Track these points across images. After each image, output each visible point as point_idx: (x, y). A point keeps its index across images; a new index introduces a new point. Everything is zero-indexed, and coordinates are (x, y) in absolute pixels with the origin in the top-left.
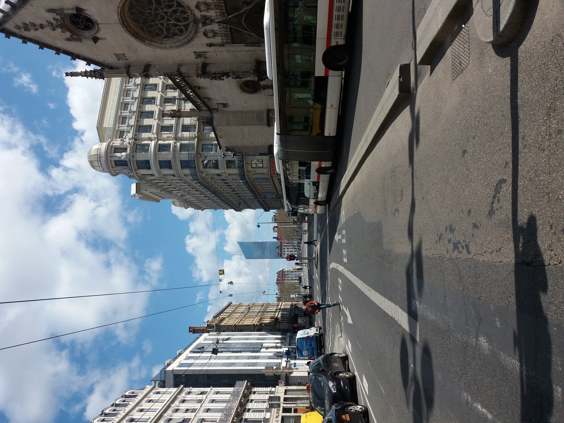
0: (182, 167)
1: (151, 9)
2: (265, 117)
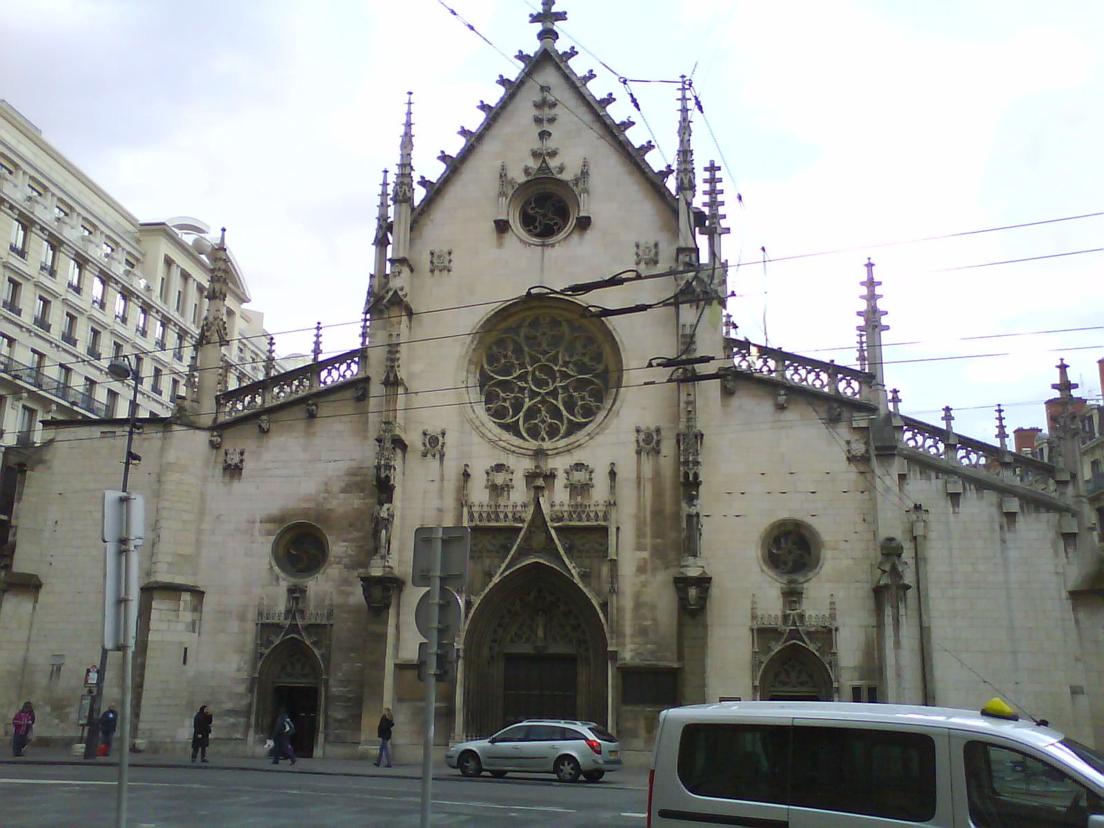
0: (1040, 450)
1: (566, 364)
2: (179, 580)
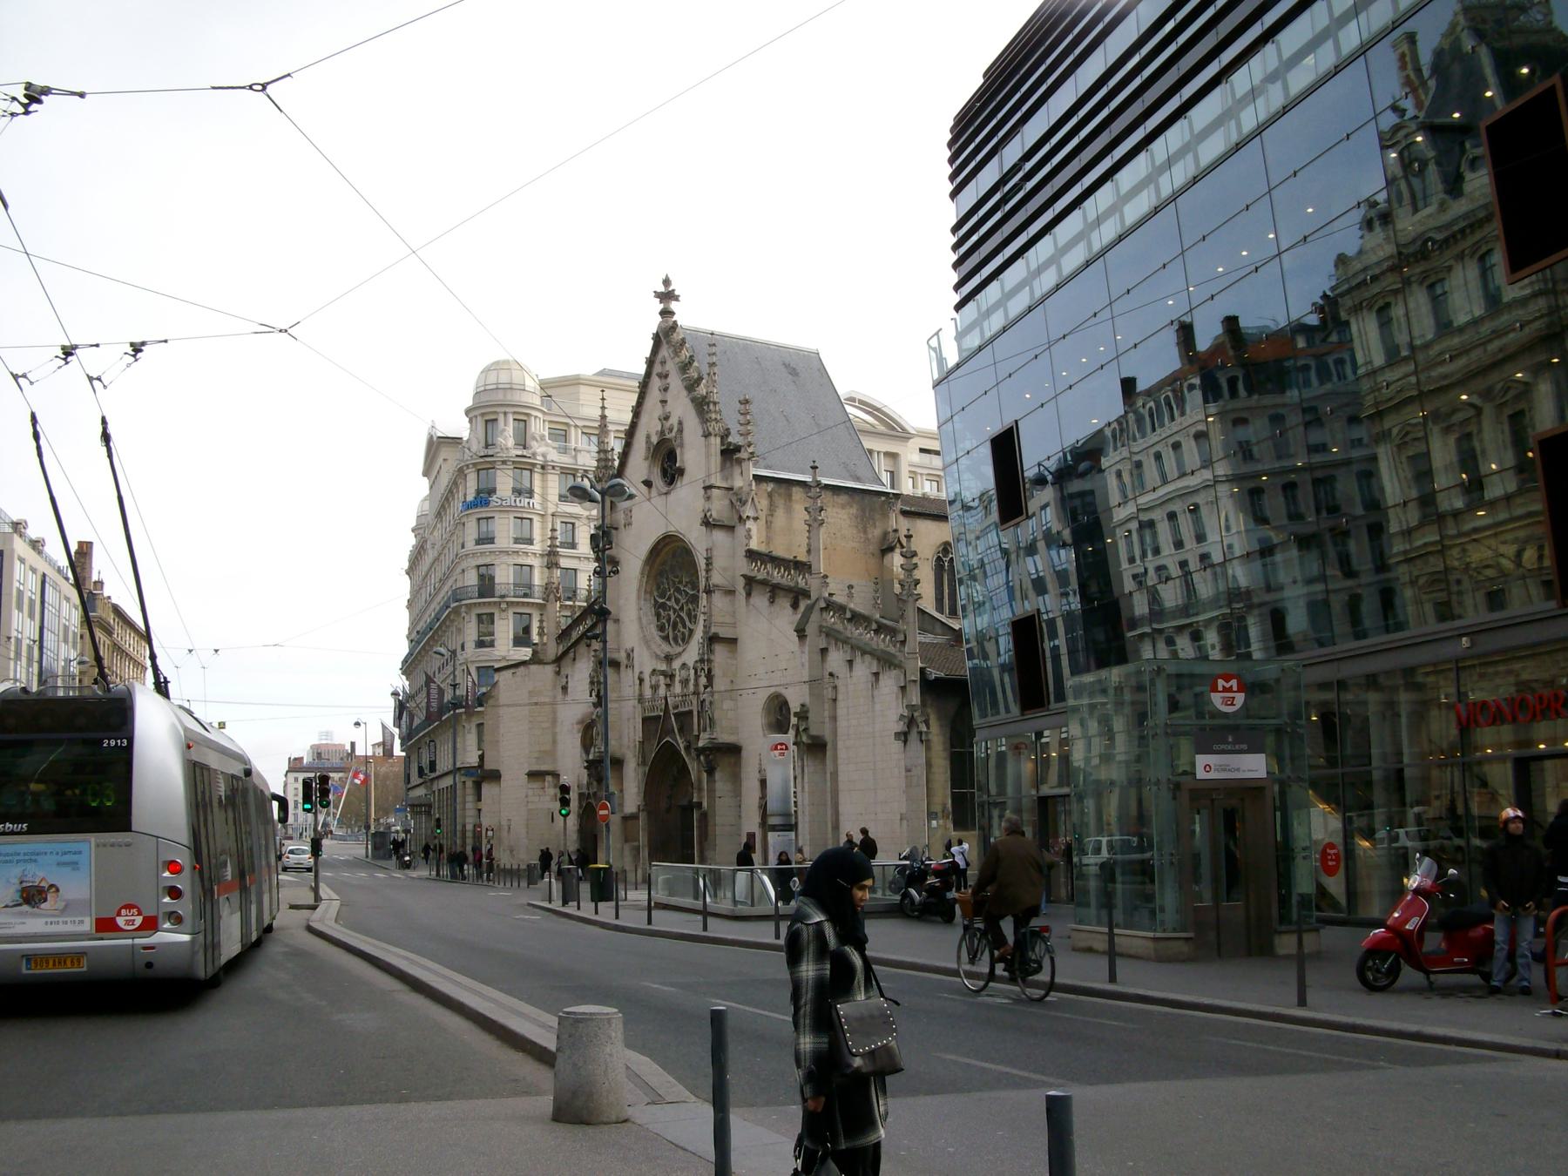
2: (544, 768)
